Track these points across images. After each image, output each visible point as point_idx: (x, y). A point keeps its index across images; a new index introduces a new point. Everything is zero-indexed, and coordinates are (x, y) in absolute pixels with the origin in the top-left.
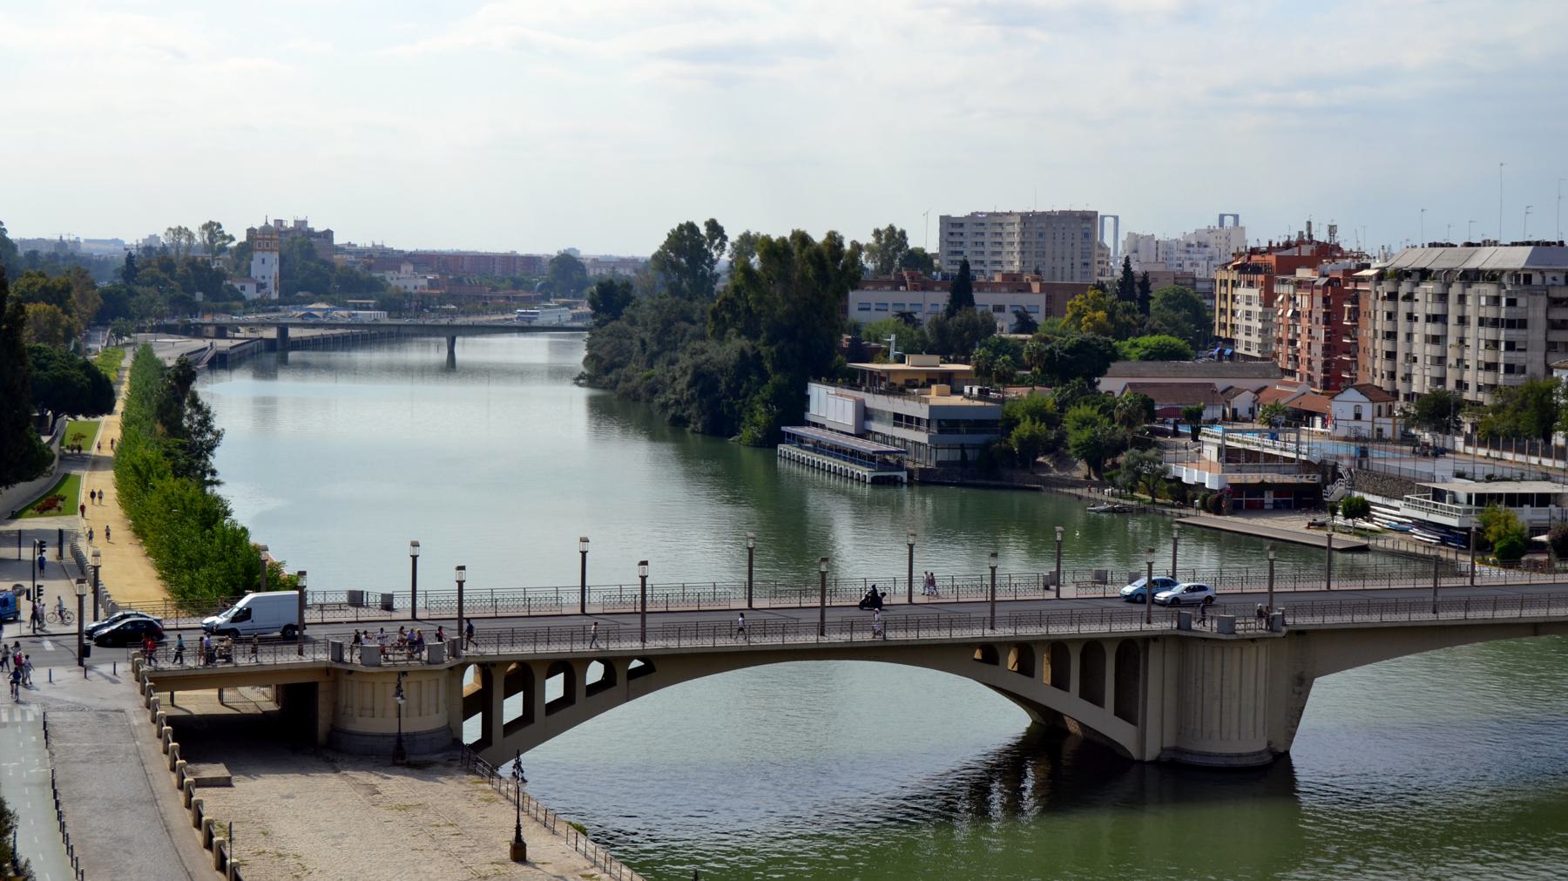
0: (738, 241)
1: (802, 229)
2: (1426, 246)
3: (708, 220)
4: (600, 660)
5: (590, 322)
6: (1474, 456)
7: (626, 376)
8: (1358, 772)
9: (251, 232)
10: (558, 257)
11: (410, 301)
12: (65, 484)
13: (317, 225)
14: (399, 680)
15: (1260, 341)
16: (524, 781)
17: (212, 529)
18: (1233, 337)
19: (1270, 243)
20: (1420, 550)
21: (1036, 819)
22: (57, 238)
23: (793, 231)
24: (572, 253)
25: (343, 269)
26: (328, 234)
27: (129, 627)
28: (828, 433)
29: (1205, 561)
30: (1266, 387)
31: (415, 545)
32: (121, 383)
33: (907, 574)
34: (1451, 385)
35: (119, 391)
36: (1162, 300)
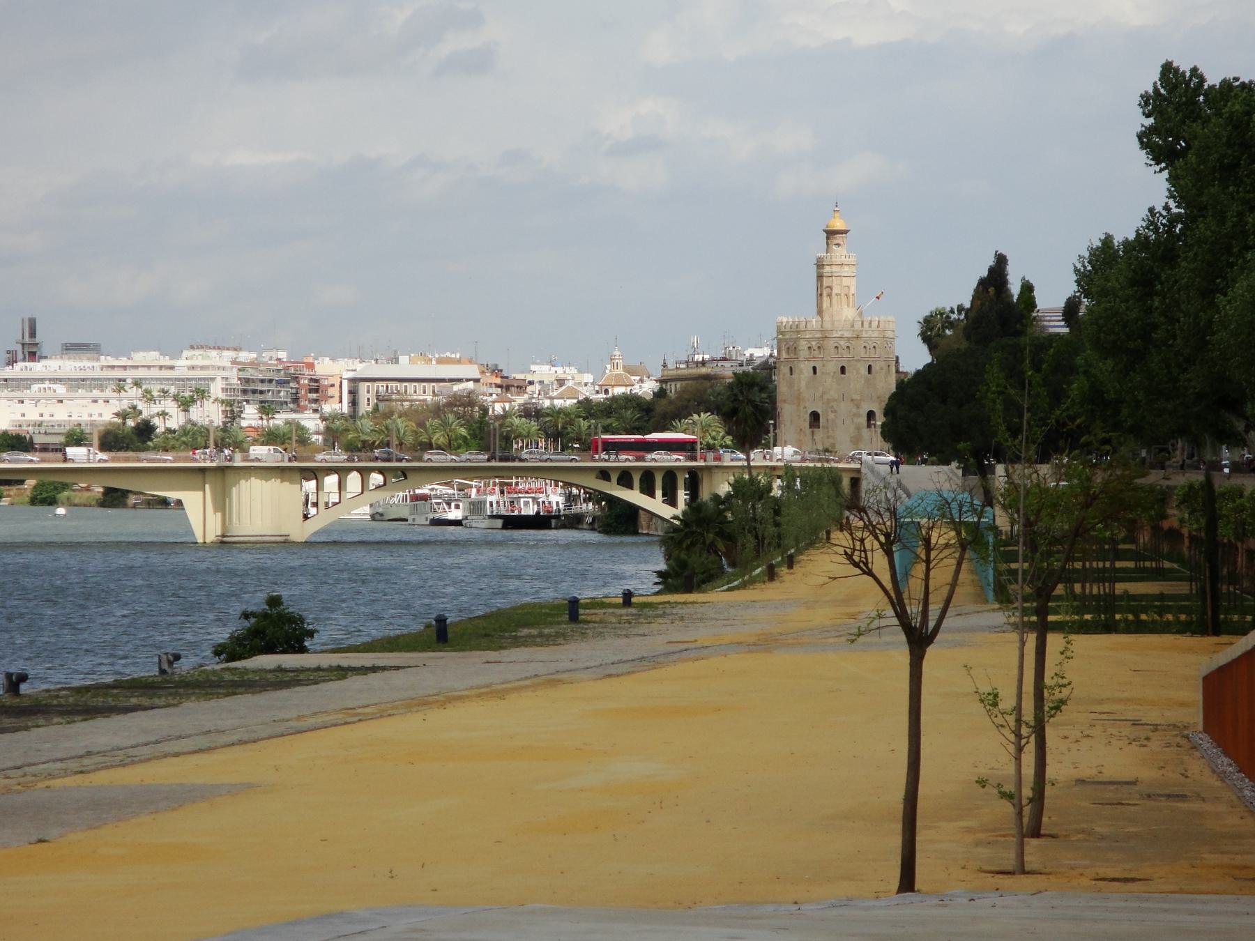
22: (285, 483)
31: (878, 298)
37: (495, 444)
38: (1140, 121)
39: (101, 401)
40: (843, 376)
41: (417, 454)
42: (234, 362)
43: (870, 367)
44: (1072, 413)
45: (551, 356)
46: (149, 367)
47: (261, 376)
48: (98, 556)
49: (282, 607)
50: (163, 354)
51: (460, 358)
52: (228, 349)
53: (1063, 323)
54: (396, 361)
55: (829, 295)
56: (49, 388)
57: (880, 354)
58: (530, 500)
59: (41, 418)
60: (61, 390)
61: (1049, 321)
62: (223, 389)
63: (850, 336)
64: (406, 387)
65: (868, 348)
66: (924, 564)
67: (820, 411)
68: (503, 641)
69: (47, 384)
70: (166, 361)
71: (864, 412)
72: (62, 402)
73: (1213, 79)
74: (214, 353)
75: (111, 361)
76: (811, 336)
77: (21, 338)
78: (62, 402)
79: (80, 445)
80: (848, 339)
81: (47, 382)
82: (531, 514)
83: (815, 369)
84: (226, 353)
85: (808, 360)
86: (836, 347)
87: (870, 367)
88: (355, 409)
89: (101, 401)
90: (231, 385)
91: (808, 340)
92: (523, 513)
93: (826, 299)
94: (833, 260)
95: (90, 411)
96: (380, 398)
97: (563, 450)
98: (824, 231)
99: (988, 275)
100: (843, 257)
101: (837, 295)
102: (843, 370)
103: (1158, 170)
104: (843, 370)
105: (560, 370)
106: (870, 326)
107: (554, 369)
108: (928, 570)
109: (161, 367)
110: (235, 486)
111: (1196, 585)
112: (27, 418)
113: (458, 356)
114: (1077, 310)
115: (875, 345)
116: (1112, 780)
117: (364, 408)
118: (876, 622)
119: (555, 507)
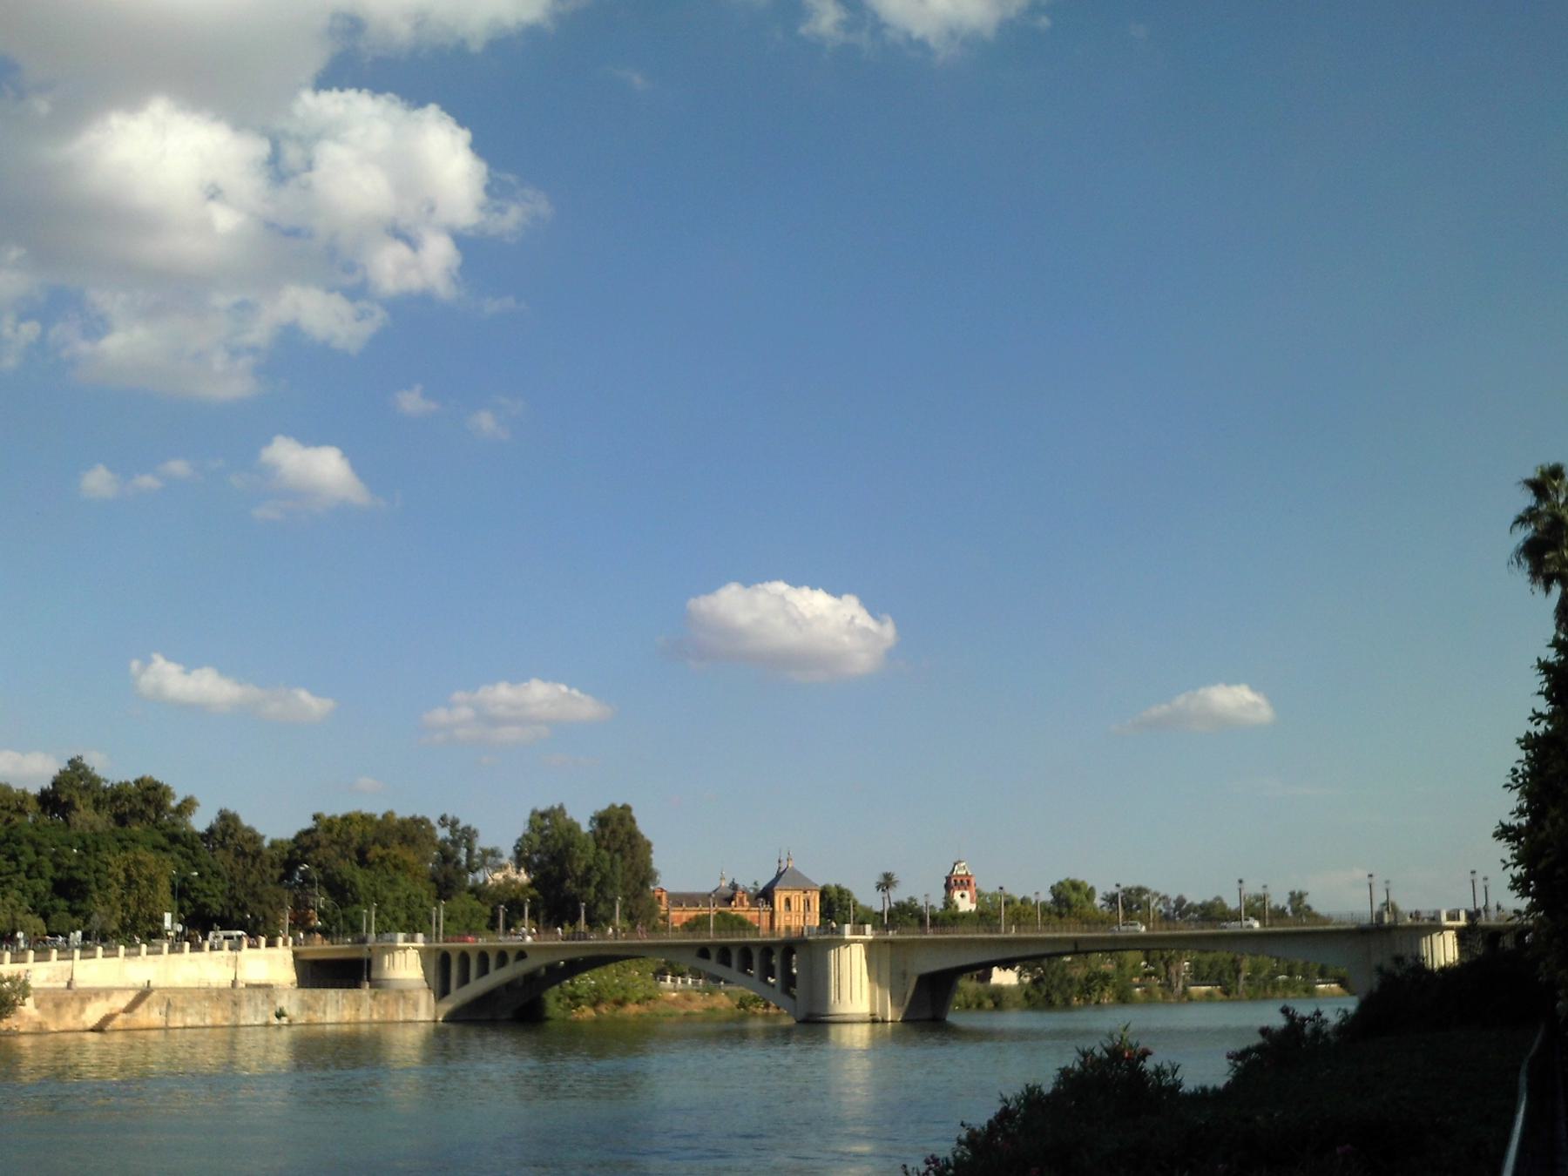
0: (1277, 1032)
1: (427, 816)
2: (1486, 883)
3: (634, 814)
4: (760, 897)
5: (391, 955)
6: (166, 1029)
7: (252, 873)
8: (765, 1152)
9: (228, 821)
10: (651, 870)
11: (338, 931)
12: (263, 982)
13: (1516, 756)
14: (1396, 918)
15: (242, 858)
16: (734, 887)
17: (949, 902)
18: (118, 1064)
19: (1517, 897)
20: (338, 1087)
21: (1438, 913)
23: (1218, 898)
24: (1527, 539)
25: (995, 1117)
26: (1529, 742)
27: (1344, 1023)
28: (1138, 947)
29: (669, 981)
30: (790, 909)
31: (1241, 881)
32: (1244, 986)
33: (1369, 893)
34: (679, 980)
35: (787, 1053)
36: (1124, 891)
38: (653, 848)
44: (581, 1017)
48: (134, 912)
49: (603, 925)
50: (748, 988)
51: (887, 931)
53: (837, 950)
61: (1426, 942)
64: (256, 1020)
66: (164, 1024)
68: (98, 1075)
73: (339, 816)
79: (822, 915)
95: (960, 898)
96: (1097, 984)
99: (1223, 1089)
103: (202, 894)
108: (328, 1024)
110: (1426, 936)
111: (1319, 984)
114: (1182, 906)
116: (67, 1029)
118: (333, 852)
119: (639, 1046)
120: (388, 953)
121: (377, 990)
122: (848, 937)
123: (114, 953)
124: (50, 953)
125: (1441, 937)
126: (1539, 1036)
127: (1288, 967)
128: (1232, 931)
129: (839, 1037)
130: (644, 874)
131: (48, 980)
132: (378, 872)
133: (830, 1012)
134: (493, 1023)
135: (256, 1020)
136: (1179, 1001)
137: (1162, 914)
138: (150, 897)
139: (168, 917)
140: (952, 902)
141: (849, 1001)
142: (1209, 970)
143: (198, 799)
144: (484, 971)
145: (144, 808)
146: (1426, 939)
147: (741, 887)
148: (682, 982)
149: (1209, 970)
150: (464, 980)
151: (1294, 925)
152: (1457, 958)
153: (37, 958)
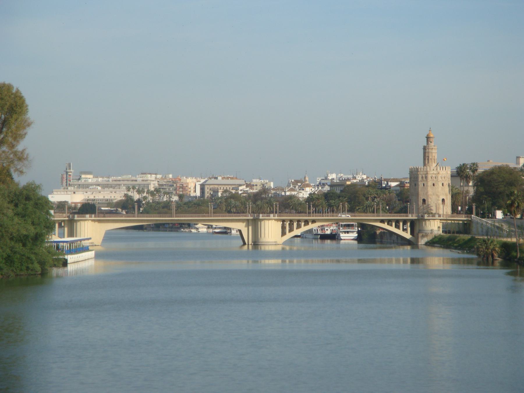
5: (425, 222)
37: (174, 209)
39: (113, 192)
40: (434, 187)
41: (269, 214)
42: (156, 178)
43: (443, 184)
45: (259, 176)
46: (128, 180)
47: (165, 183)
51: (233, 177)
52: (153, 174)
54: (216, 178)
55: (428, 159)
56: (96, 188)
57: (446, 179)
58: (330, 229)
59: (94, 198)
60: (99, 188)
62: (114, 189)
63: (436, 173)
65: (442, 177)
67: (426, 199)
69: (94, 186)
70: (134, 178)
71: (441, 199)
72: (100, 192)
74: (149, 176)
75: (115, 178)
76: (422, 173)
77: (65, 169)
78: (100, 192)
80: (436, 174)
81: (95, 186)
82: (329, 233)
83: (424, 184)
84: (154, 176)
85: (421, 181)
86: (431, 177)
87: (443, 184)
88: (203, 195)
89: (113, 192)
90: (155, 186)
91: (422, 174)
92: (326, 233)
93: (427, 161)
94: (430, 147)
97: (169, 209)
98: (426, 137)
100: (433, 146)
101: (431, 159)
102: (434, 185)
104: (434, 185)
105: (263, 181)
106: (424, 170)
107: (260, 181)
109: (132, 181)
112: (89, 198)
113: (232, 177)
115: (442, 176)
117: (207, 195)
120: (424, 221)
121: (429, 198)
122: (426, 218)
123: (132, 215)
124: (519, 257)
125: (429, 222)
126: (107, 209)
127: (37, 234)
128: (460, 251)
129: (261, 248)
130: (122, 197)
131: (420, 197)
132: (14, 200)
133: (259, 241)
134: (429, 245)
135: (230, 187)
136: (459, 214)
137: (33, 204)
138: (472, 168)
139: (120, 178)
140: (311, 199)
141: (90, 241)
142: (34, 253)
143: (92, 238)
144: (299, 227)
145: (17, 248)
146: (79, 223)
147: (325, 183)
148: (290, 262)
149: (34, 253)
150: (291, 230)
151: (384, 211)
152: (330, 232)
153: (68, 212)
